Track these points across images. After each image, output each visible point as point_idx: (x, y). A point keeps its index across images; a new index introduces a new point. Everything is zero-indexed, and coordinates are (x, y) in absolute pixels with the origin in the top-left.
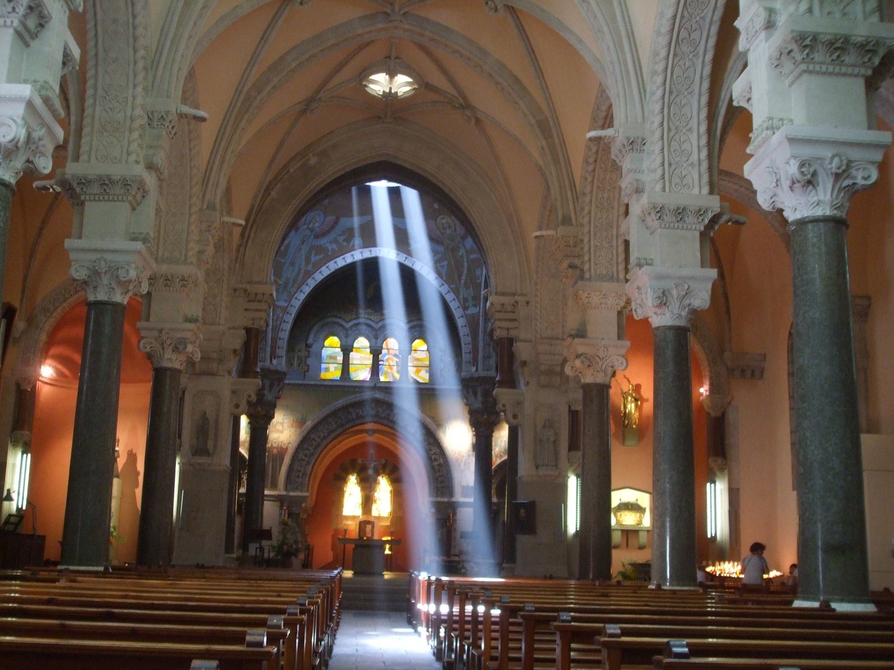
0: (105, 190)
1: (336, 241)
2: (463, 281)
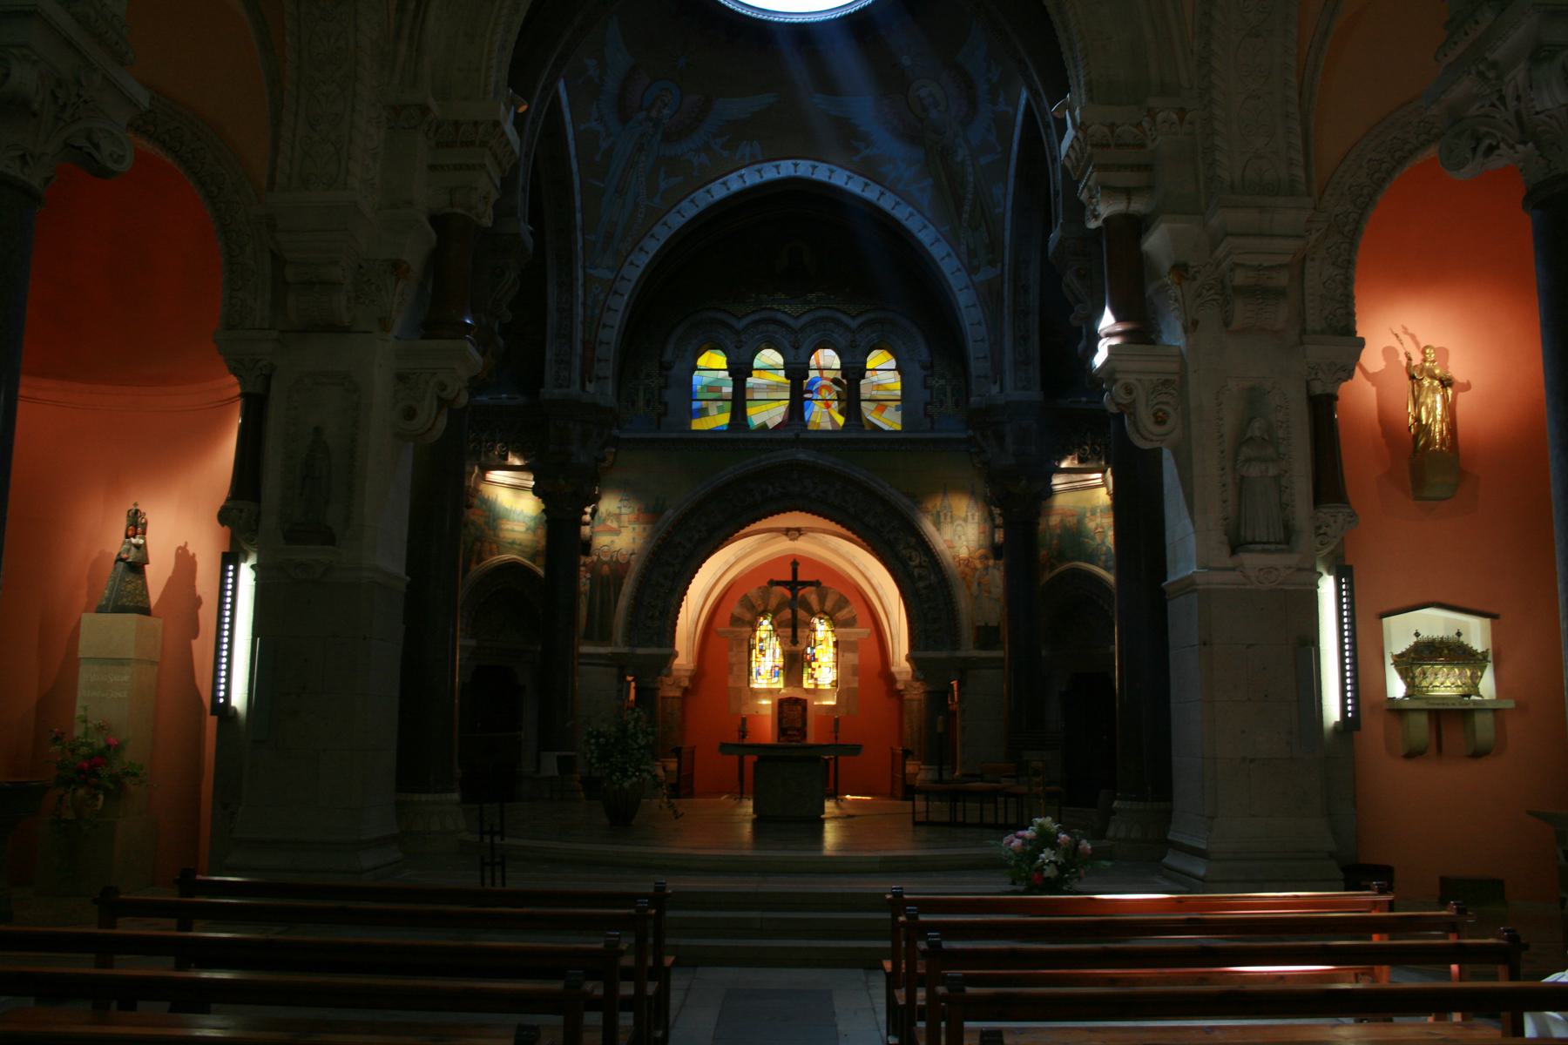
2: (965, 216)
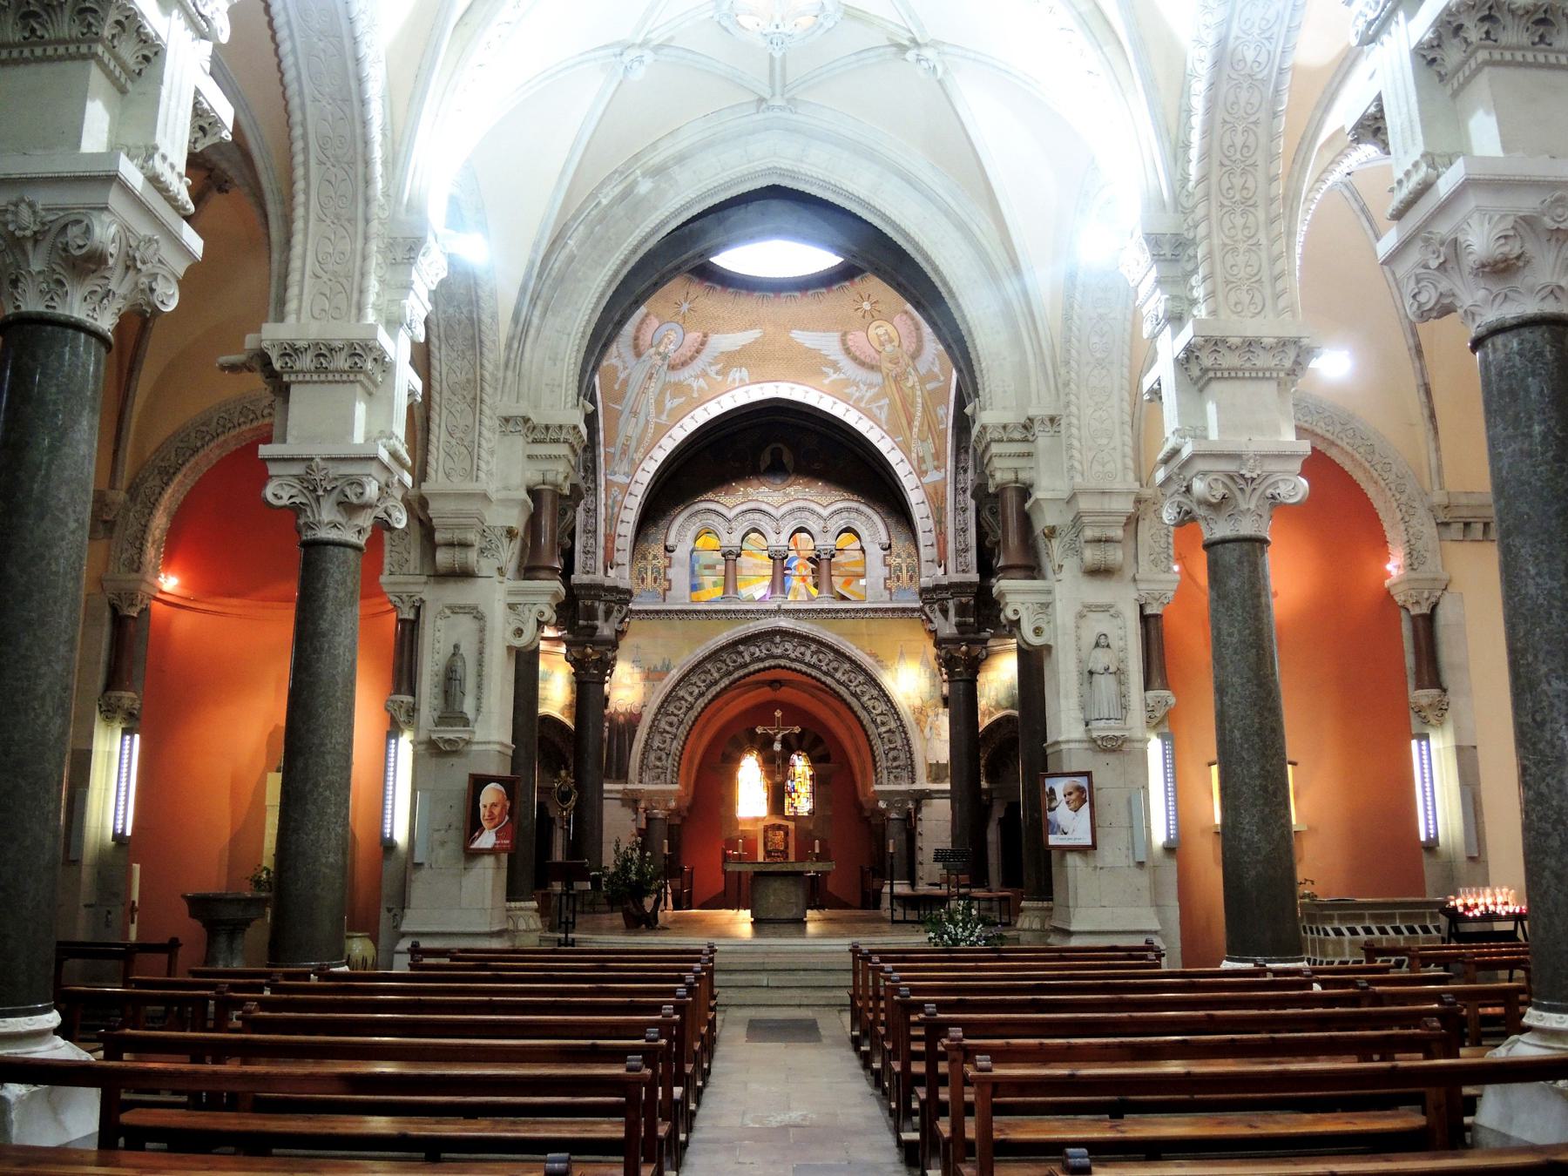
0: (33, 31)
1: (704, 374)
2: (915, 430)
